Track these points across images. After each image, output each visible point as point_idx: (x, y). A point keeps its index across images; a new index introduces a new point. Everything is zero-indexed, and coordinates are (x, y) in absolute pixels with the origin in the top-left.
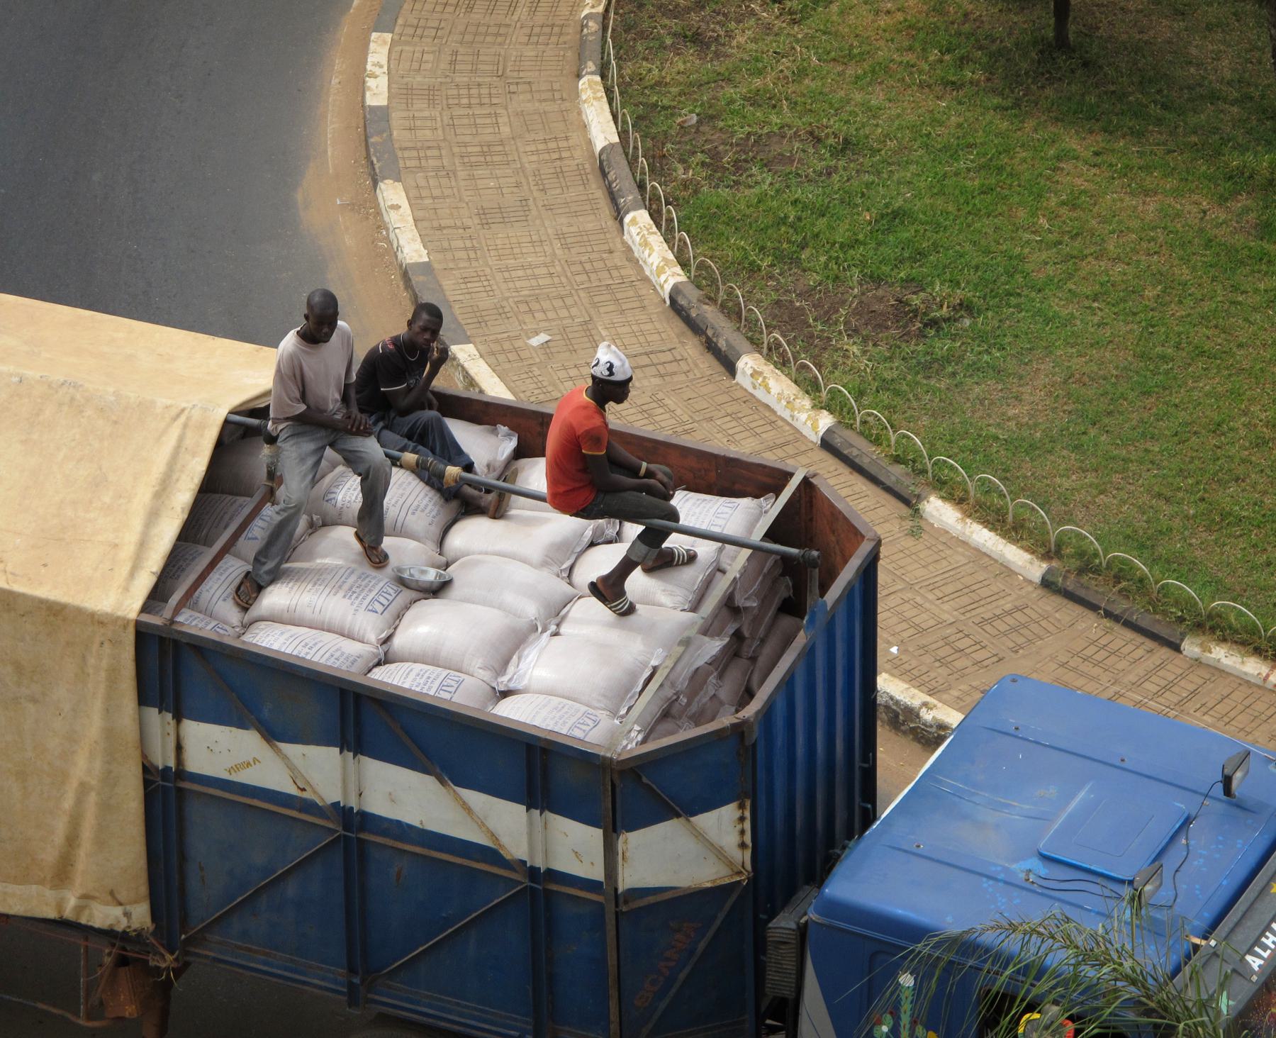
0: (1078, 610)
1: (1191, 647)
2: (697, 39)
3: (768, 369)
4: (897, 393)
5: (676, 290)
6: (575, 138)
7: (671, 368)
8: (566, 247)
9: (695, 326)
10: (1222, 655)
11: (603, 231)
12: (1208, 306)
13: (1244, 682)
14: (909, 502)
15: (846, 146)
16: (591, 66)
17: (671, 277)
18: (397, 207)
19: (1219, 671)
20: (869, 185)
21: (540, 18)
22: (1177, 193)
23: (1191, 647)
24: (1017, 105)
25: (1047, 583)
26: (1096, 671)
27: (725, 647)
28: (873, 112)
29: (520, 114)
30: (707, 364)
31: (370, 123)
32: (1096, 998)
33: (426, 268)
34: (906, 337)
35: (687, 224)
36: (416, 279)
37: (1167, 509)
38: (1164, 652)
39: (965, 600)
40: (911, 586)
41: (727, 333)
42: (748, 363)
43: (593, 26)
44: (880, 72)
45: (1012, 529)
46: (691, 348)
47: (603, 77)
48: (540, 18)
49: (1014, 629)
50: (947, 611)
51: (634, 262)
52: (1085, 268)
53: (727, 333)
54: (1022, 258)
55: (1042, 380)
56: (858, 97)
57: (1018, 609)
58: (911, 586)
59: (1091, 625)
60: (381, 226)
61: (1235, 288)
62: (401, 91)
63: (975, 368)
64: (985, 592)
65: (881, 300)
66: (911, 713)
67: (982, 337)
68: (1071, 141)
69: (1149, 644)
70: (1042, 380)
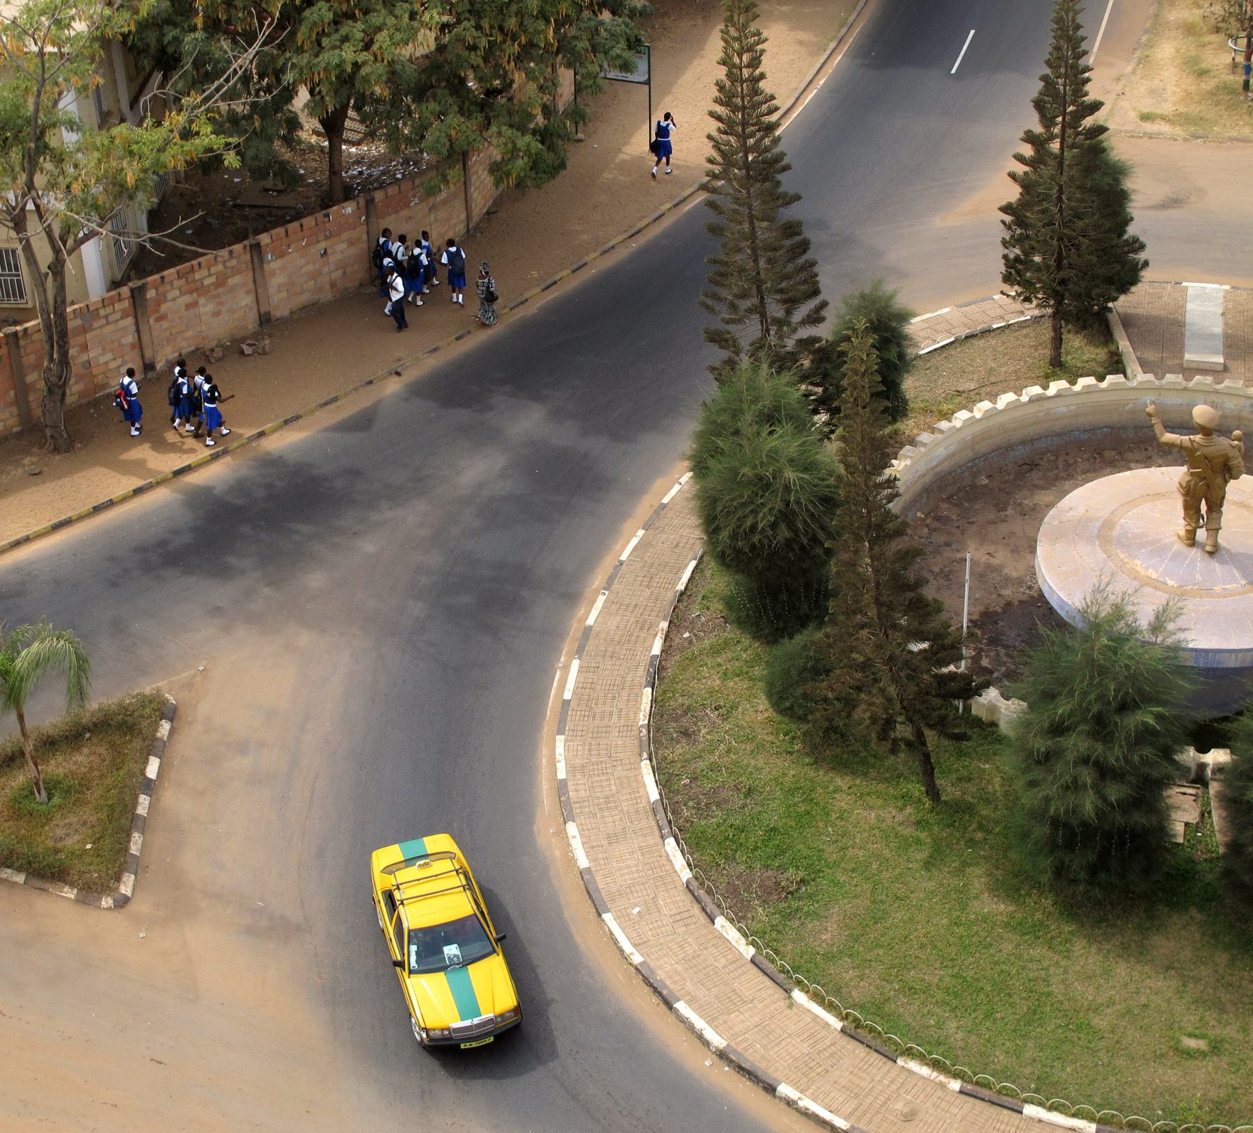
0: (857, 1043)
1: (900, 1061)
2: (686, 734)
3: (728, 924)
4: (779, 932)
5: (688, 882)
6: (641, 790)
7: (689, 921)
8: (643, 855)
9: (697, 900)
10: (913, 1065)
11: (657, 845)
12: (898, 871)
13: (923, 1077)
14: (788, 991)
15: (749, 792)
16: (645, 755)
17: (686, 874)
18: (574, 837)
19: (909, 1071)
20: (760, 812)
21: (622, 721)
22: (882, 807)
23: (900, 1061)
24: (816, 762)
25: (843, 1031)
26: (864, 1075)
27: (626, 143)
28: (759, 770)
29: (619, 778)
30: (702, 918)
31: (562, 787)
32: (856, 1020)
33: (588, 870)
34: (780, 900)
35: (692, 842)
36: (586, 877)
37: (888, 987)
38: (890, 1063)
39: (812, 1041)
40: (790, 1036)
41: (711, 907)
42: (720, 921)
43: (645, 731)
44: (760, 747)
45: (830, 1007)
46: (696, 910)
47: (651, 760)
48: (622, 721)
49: (832, 1055)
50: (805, 1048)
51: (670, 861)
52: (850, 852)
53: (711, 907)
54: (823, 851)
55: (835, 918)
56: (753, 762)
57: (832, 1044)
58: (790, 1036)
59: (861, 1050)
60: (569, 845)
61: (908, 860)
62: (571, 769)
63: (808, 914)
64: (819, 1036)
65: (769, 878)
66: (795, 1102)
67: (810, 896)
68: (839, 781)
69: (884, 1059)
70: (835, 918)
